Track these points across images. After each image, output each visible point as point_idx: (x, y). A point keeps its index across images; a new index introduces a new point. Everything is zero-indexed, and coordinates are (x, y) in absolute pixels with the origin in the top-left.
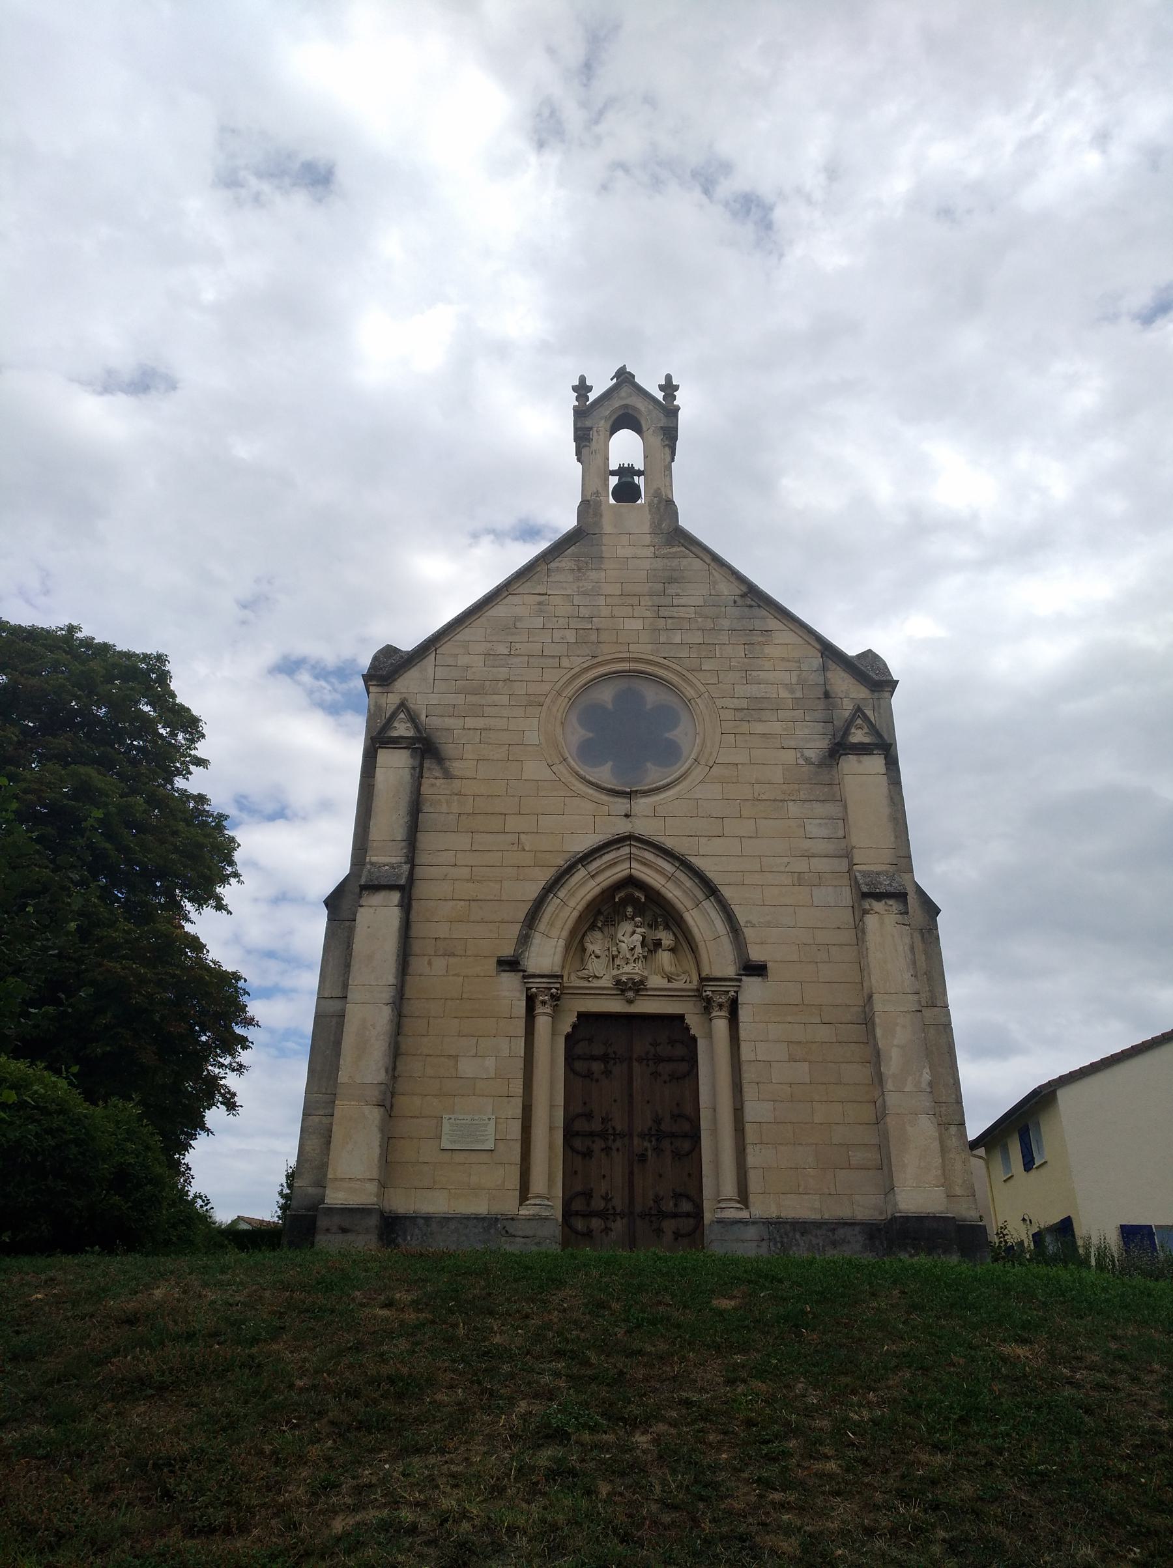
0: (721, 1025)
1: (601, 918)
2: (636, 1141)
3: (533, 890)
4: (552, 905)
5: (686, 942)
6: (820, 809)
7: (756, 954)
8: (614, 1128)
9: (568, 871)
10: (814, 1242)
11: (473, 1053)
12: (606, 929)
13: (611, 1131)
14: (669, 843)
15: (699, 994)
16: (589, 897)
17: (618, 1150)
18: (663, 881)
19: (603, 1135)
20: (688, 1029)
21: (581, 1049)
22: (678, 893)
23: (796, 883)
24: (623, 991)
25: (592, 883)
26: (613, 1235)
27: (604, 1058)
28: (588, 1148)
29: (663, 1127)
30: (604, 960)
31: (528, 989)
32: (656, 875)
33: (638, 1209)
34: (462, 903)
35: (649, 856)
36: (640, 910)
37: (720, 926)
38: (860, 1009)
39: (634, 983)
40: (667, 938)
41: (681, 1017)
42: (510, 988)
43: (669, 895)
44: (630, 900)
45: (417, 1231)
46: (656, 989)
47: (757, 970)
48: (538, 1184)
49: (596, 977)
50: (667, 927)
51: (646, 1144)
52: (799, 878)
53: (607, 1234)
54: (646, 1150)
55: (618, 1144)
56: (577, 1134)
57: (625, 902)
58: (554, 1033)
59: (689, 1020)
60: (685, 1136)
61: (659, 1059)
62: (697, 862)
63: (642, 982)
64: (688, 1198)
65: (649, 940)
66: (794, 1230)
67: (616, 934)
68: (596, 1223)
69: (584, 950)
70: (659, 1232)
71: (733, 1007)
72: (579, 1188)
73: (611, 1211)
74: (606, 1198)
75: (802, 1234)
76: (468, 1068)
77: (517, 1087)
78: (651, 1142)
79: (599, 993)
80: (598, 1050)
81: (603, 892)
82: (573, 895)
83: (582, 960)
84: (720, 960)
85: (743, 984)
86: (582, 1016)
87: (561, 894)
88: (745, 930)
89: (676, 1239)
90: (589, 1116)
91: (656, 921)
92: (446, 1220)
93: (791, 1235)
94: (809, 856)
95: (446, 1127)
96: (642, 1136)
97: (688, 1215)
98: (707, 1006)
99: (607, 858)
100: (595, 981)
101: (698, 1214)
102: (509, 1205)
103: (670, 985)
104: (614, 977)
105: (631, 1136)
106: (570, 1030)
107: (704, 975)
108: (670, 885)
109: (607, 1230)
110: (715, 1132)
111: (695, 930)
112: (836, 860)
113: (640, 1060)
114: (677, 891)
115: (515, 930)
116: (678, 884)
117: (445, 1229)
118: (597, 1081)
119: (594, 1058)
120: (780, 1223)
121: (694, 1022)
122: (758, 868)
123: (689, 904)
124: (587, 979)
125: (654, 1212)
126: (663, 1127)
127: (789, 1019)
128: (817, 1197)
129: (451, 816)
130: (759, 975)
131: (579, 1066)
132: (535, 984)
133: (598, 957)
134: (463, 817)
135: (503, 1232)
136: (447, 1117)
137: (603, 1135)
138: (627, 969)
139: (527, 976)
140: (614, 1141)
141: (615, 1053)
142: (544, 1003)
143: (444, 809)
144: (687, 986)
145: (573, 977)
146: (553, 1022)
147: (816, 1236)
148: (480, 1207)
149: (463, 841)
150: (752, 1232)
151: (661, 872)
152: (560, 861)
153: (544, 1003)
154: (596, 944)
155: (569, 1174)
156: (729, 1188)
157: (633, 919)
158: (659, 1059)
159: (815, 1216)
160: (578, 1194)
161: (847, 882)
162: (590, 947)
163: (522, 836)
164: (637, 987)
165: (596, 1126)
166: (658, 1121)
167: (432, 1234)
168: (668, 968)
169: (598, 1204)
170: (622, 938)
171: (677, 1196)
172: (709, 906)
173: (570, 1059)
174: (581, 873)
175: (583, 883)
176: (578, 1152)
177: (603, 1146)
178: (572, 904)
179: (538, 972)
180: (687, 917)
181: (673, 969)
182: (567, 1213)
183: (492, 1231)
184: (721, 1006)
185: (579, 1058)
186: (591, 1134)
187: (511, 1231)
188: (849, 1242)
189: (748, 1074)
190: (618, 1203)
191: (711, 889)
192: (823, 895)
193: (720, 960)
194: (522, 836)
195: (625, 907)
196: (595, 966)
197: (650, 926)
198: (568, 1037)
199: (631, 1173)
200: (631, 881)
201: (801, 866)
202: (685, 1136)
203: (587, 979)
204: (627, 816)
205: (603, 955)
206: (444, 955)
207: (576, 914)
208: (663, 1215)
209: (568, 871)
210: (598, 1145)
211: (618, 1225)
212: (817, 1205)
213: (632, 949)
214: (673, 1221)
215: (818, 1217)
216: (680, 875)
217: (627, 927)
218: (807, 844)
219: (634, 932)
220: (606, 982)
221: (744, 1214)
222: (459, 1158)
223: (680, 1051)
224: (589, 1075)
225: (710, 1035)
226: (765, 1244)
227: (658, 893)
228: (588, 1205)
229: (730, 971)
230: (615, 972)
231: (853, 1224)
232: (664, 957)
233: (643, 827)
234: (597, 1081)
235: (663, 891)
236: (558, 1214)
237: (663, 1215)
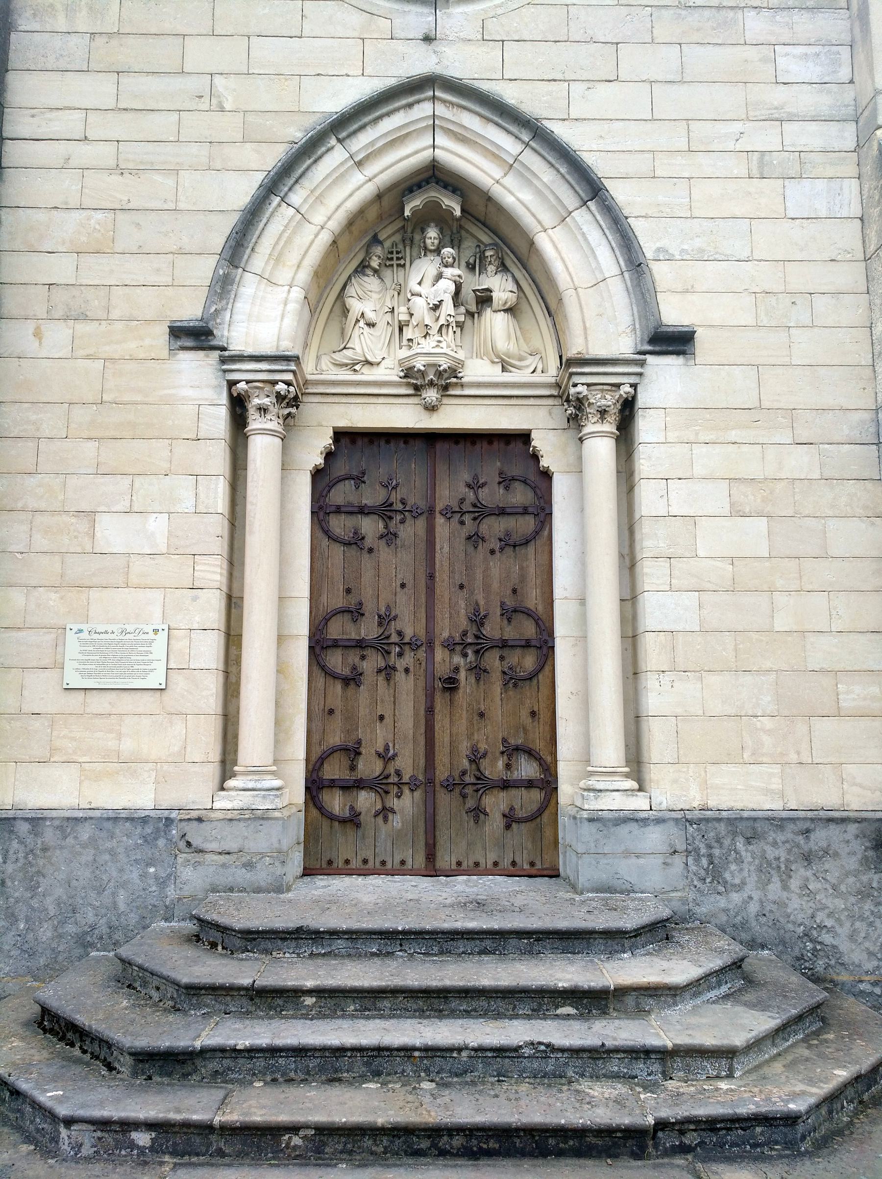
0: (601, 449)
1: (378, 250)
2: (440, 654)
3: (241, 191)
4: (278, 220)
5: (540, 293)
6: (806, 25)
7: (674, 314)
8: (400, 633)
9: (309, 149)
10: (771, 853)
11: (123, 505)
12: (387, 274)
13: (394, 638)
14: (510, 95)
15: (561, 394)
16: (352, 204)
17: (407, 670)
18: (497, 172)
19: (382, 646)
20: (535, 457)
21: (341, 494)
22: (527, 196)
23: (755, 173)
24: (417, 388)
25: (358, 177)
26: (396, 822)
27: (385, 511)
28: (354, 668)
29: (487, 630)
30: (383, 332)
31: (232, 384)
32: (485, 159)
33: (442, 773)
34: (99, 215)
35: (471, 121)
36: (453, 233)
37: (608, 260)
38: (867, 416)
39: (440, 374)
40: (502, 288)
41: (525, 437)
42: (196, 380)
43: (508, 200)
44: (432, 214)
45: (15, 844)
46: (479, 385)
47: (674, 342)
48: (254, 746)
49: (368, 363)
50: (503, 268)
51: (458, 659)
52: (761, 164)
53: (386, 819)
54: (457, 669)
55: (408, 659)
56: (335, 644)
57: (421, 221)
58: (286, 466)
59: (538, 441)
60: (527, 645)
61: (480, 512)
62: (560, 130)
63: (453, 372)
64: (530, 753)
65: (467, 293)
66: (734, 834)
67: (406, 280)
68: (365, 800)
69: (345, 311)
70: (478, 813)
71: (628, 409)
72: (336, 739)
73: (393, 779)
74: (386, 757)
75: (748, 840)
76: (113, 533)
77: (214, 572)
78: (465, 655)
79: (373, 394)
80: (372, 496)
81: (379, 196)
82: (320, 199)
83: (343, 332)
84: (604, 326)
85: (647, 370)
86: (340, 435)
87: (296, 198)
88: (655, 267)
89: (508, 827)
90: (356, 613)
91: (483, 258)
92: (71, 823)
93: (727, 842)
94: (780, 119)
95: (72, 647)
96: (450, 646)
97: (530, 784)
98: (576, 412)
99: (387, 125)
100: (366, 370)
101: (548, 784)
102: (195, 790)
103: (507, 377)
104: (401, 362)
105: (430, 645)
106: (320, 461)
107: (574, 349)
108: (510, 181)
109: (385, 812)
110: (583, 639)
111: (558, 269)
112: (834, 127)
113: (448, 513)
114: (524, 192)
115: (204, 269)
116: (527, 177)
117: (70, 841)
118: (371, 550)
119: (363, 511)
120: (707, 820)
121: (549, 447)
122: (683, 145)
123: (547, 218)
124: (351, 366)
125: (468, 779)
126: (487, 630)
127: (733, 435)
128: (776, 769)
129: (74, 40)
130: (678, 353)
131: (339, 525)
132: (244, 372)
133: (371, 325)
134: (100, 41)
135: (182, 845)
136: (75, 628)
137: (382, 646)
138: (428, 345)
139: (228, 359)
140: (400, 655)
141: (403, 501)
142: (263, 410)
143: (61, 24)
144: (538, 378)
145: (325, 363)
146: (285, 450)
147: (775, 844)
148: (140, 795)
149: (98, 90)
150: (654, 839)
151: (494, 154)
152: (297, 133)
153: (263, 410)
154: (368, 298)
155: (319, 715)
156: (610, 751)
157: (438, 251)
158: (480, 512)
159: (770, 804)
160: (333, 751)
161: (853, 170)
162: (356, 306)
163: (217, 80)
164: (447, 381)
165: (368, 630)
166: (478, 620)
167: (45, 849)
168: (502, 345)
169: (369, 767)
170: (417, 289)
171: (512, 751)
172: (587, 221)
173: (321, 511)
174: (335, 157)
175: (339, 178)
176: (335, 676)
177: (382, 664)
178: (318, 218)
179: (250, 351)
180: (543, 242)
181: (512, 347)
182: (315, 786)
183: (161, 842)
184: (603, 413)
185: (338, 510)
186: (360, 645)
187: (196, 842)
188: (836, 855)
189: (651, 541)
190: (408, 763)
191: (591, 188)
192: (805, 196)
193: (604, 326)
194: (217, 80)
195: (423, 230)
196: (365, 343)
197: (471, 267)
198: (317, 474)
199: (430, 710)
200: (434, 175)
201: (766, 138)
202: (527, 645)
203: (351, 366)
204: (428, 39)
205: (382, 320)
206: (66, 318)
207: (325, 238)
208: (483, 784)
209: (309, 149)
210: (371, 663)
211: (406, 805)
212: (776, 784)
213: (436, 308)
214: (502, 795)
215: (777, 805)
216: (531, 159)
217: (427, 267)
218: (779, 95)
219: (439, 276)
220: (388, 372)
221: (639, 803)
222: (99, 703)
223: (520, 496)
224: (356, 541)
225: (578, 469)
226: (678, 860)
227: (488, 199)
228: (353, 768)
229: (624, 344)
230: (404, 353)
231: (843, 820)
232: (496, 323)
233: (457, 62)
234: (371, 550)
235: (497, 191)
236: (297, 794)
237: (483, 784)
